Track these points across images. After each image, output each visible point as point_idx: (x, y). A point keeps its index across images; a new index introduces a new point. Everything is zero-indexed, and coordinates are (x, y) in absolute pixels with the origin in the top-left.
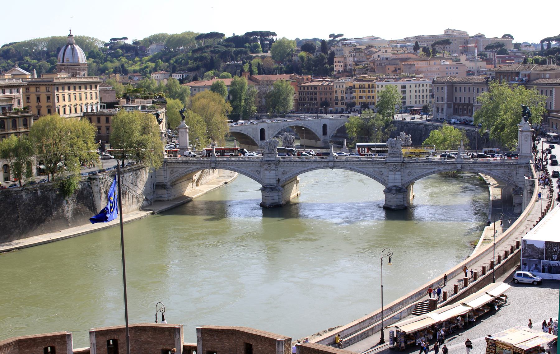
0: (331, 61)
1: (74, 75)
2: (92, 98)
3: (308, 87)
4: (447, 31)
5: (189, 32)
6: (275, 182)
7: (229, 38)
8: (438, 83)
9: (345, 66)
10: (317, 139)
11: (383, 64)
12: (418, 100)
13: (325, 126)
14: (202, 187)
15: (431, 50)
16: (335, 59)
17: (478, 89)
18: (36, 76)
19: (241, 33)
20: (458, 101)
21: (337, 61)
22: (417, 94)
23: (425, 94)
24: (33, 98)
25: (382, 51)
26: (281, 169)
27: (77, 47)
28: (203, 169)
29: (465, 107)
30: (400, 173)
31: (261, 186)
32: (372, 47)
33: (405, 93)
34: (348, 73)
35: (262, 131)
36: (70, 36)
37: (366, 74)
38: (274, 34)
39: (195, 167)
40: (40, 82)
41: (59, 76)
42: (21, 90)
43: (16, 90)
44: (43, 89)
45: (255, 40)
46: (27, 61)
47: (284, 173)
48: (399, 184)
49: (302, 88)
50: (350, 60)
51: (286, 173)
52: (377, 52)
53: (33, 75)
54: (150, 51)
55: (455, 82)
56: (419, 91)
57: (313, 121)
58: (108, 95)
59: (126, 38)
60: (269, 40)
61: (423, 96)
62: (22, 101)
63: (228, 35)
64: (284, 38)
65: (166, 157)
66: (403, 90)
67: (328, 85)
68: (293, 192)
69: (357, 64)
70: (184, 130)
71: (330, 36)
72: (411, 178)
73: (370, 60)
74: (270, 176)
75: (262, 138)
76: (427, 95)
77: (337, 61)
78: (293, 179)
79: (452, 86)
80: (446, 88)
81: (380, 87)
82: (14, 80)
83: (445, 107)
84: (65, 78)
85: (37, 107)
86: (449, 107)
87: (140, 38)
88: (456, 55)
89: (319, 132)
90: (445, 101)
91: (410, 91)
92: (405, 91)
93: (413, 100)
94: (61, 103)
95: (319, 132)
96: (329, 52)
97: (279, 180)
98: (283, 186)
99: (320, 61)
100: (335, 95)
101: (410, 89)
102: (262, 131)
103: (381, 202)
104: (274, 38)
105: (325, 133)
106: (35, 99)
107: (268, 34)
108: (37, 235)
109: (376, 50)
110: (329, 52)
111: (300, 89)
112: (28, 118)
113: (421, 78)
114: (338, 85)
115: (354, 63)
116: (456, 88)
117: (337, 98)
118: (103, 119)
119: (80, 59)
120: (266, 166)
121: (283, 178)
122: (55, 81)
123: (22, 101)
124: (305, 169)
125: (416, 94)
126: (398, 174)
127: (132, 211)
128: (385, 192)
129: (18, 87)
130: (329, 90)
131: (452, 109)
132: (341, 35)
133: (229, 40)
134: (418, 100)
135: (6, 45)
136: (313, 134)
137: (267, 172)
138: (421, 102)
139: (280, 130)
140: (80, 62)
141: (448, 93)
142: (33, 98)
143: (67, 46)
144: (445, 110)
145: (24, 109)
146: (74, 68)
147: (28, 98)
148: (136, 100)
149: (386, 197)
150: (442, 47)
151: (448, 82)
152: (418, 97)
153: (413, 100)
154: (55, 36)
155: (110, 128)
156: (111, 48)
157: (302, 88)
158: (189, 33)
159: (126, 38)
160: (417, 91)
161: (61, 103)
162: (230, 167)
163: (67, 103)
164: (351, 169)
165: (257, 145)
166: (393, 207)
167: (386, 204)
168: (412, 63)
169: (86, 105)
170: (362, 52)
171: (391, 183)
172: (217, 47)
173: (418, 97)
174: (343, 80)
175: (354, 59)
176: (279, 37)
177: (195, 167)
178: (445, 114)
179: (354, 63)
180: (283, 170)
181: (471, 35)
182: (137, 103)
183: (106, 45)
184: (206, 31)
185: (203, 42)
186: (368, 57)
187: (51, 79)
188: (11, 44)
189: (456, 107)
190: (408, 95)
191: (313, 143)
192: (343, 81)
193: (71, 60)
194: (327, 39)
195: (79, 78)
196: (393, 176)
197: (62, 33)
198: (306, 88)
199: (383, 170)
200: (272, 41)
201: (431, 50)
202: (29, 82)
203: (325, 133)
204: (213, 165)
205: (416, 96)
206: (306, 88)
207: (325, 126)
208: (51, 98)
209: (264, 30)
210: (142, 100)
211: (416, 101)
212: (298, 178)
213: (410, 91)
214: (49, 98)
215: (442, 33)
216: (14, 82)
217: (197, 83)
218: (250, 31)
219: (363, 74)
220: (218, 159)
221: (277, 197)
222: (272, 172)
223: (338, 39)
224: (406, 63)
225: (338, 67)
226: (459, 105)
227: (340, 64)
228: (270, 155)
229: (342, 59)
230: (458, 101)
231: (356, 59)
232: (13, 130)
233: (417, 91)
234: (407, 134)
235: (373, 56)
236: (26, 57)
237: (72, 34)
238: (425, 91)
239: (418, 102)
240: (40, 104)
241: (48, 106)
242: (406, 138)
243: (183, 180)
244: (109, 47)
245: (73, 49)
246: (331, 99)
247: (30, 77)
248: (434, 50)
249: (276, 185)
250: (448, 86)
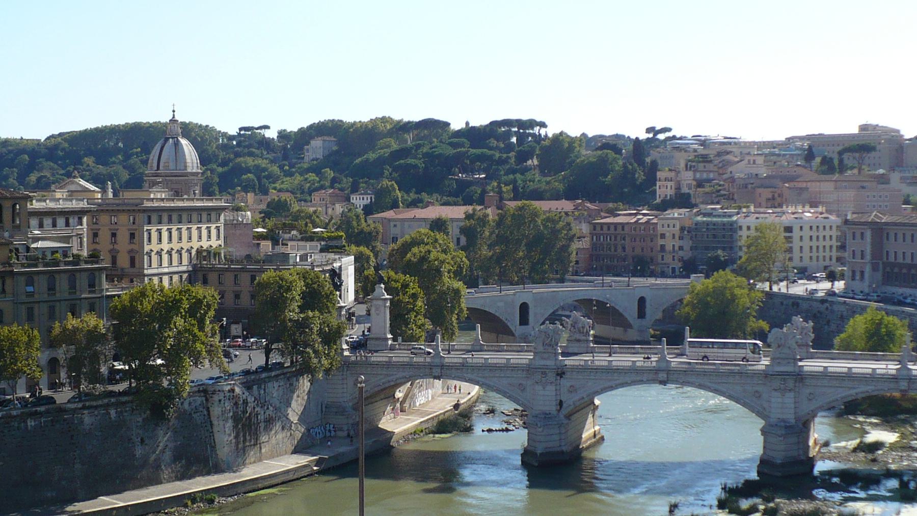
0: (652, 179)
1: (177, 194)
2: (209, 237)
3: (609, 225)
4: (864, 128)
5: (384, 118)
6: (554, 408)
7: (459, 131)
8: (855, 223)
9: (678, 188)
10: (626, 325)
11: (750, 186)
12: (814, 254)
13: (642, 301)
14: (415, 411)
15: (836, 162)
16: (659, 174)
17: (854, 233)
18: (111, 195)
19: (480, 120)
20: (892, 259)
21: (663, 178)
22: (814, 243)
23: (828, 243)
24: (105, 235)
25: (746, 161)
26: (565, 383)
27: (184, 142)
28: (411, 379)
29: (896, 270)
30: (792, 394)
31: (761, 423)
32: (728, 153)
33: (791, 242)
34: (682, 200)
35: (524, 308)
36: (173, 121)
37: (718, 203)
38: (543, 125)
39: (401, 374)
40: (118, 205)
41: (152, 196)
42: (85, 220)
43: (76, 219)
44: (123, 218)
45: (508, 134)
46: (88, 165)
47: (572, 390)
48: (790, 417)
49: (598, 228)
50: (687, 178)
51: (576, 391)
52: (738, 162)
53: (104, 191)
54: (311, 151)
55: (886, 224)
56: (818, 237)
57: (621, 290)
58: (238, 232)
59: (267, 127)
60: (534, 135)
61: (818, 247)
62: (85, 239)
63: (457, 125)
64: (561, 133)
65: (346, 353)
66: (788, 234)
67: (648, 222)
68: (587, 427)
69: (700, 184)
70: (380, 303)
71: (649, 130)
72: (813, 407)
73: (725, 176)
74: (544, 397)
75: (524, 321)
76: (831, 247)
77: (663, 178)
78: (588, 405)
79: (880, 231)
80: (868, 234)
81: (745, 228)
82: (74, 202)
83: (868, 269)
84: (162, 200)
85: (110, 251)
86: (875, 268)
87: (293, 127)
88: (881, 171)
89: (630, 311)
90: (868, 257)
91: (801, 237)
92: (790, 237)
93: (806, 254)
94: (154, 246)
95: (630, 311)
96: (648, 160)
97: (561, 403)
98: (568, 417)
99: (626, 176)
100: (661, 242)
101: (802, 233)
102: (524, 308)
103: (825, 420)
104: (543, 132)
105: (641, 314)
106: (108, 235)
107: (532, 123)
108: (408, 429)
109: (737, 160)
110: (648, 160)
111: (595, 229)
112: (97, 274)
113: (821, 213)
114: (666, 222)
115: (694, 183)
116: (888, 234)
117: (663, 247)
118: (229, 277)
119: (189, 165)
120: (538, 376)
121: (570, 400)
122: (148, 204)
123: (85, 239)
124: (613, 383)
125: (811, 244)
126: (789, 398)
127: (276, 458)
128: (764, 432)
129: (80, 213)
130: (648, 232)
131: (881, 272)
132: (669, 130)
133: (458, 134)
134: (814, 254)
135: (53, 136)
136: (621, 315)
137: (539, 388)
138: (821, 258)
139: (557, 307)
140: (189, 170)
141: (872, 244)
142: (105, 235)
143: (167, 140)
144: (867, 275)
145: (91, 256)
146: (178, 183)
147: (95, 235)
148: (290, 243)
149: (765, 442)
150: (857, 155)
151: (874, 223)
152: (814, 249)
153: (806, 254)
154: (139, 121)
155: (242, 296)
156: (238, 144)
157: (598, 228)
158: (384, 120)
159: (267, 127)
160: (814, 238)
161: (154, 246)
162: (469, 376)
163: (165, 246)
164: (701, 386)
165: (513, 335)
166: (779, 461)
167: (764, 453)
168: (804, 185)
169: (169, 253)
170: (710, 161)
171: (776, 414)
172: (435, 147)
173: (814, 249)
174: (676, 213)
175: (695, 176)
176: (551, 131)
177: (401, 374)
178: (867, 283)
179: (694, 183)
180: (569, 384)
181: (907, 137)
182: (292, 248)
183: (231, 138)
184: (416, 117)
185: (409, 139)
186: (721, 171)
187: (139, 201)
188: (60, 134)
189: (888, 269)
190: (796, 244)
191: (617, 332)
192: (676, 215)
193: (172, 165)
194: (643, 136)
195: (187, 199)
196: (780, 400)
197: (153, 113)
198: (605, 228)
199: (760, 389)
200: (538, 138)
201: (836, 162)
202: (99, 205)
203: (641, 314)
204: (437, 371)
205: (811, 247)
206: (605, 228)
207: (642, 301)
208: (137, 235)
209: (525, 117)
210: (301, 243)
211: (811, 258)
212: (597, 402)
213: (801, 237)
214: (132, 236)
215: (852, 129)
216: (75, 205)
217: (400, 213)
218: (499, 117)
219: (712, 203)
220: (447, 360)
221: (556, 437)
222: (788, 395)
223: (661, 137)
224: (792, 184)
225: (664, 190)
226: (893, 265)
227: (669, 184)
228: (546, 355)
229: (673, 174)
230: (892, 259)
231: (698, 175)
232: (90, 292)
233: (814, 238)
234: (806, 320)
235: (730, 169)
236: (86, 159)
237: (177, 118)
238: (828, 238)
239: (814, 259)
240: (115, 246)
241: (131, 251)
242: (803, 328)
243: (377, 399)
244: (235, 143)
245: (177, 144)
246: (652, 249)
247: (99, 196)
248: (841, 161)
249: (555, 413)
250: (872, 230)
